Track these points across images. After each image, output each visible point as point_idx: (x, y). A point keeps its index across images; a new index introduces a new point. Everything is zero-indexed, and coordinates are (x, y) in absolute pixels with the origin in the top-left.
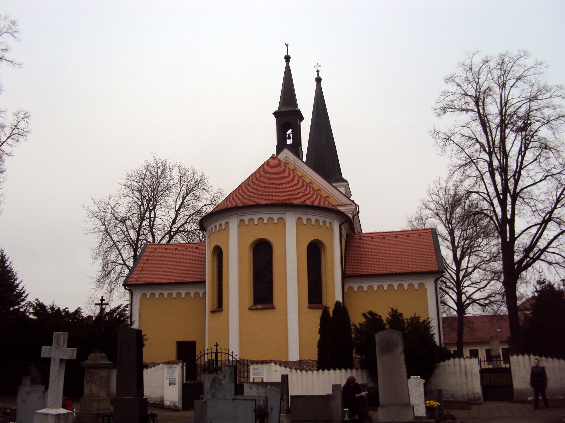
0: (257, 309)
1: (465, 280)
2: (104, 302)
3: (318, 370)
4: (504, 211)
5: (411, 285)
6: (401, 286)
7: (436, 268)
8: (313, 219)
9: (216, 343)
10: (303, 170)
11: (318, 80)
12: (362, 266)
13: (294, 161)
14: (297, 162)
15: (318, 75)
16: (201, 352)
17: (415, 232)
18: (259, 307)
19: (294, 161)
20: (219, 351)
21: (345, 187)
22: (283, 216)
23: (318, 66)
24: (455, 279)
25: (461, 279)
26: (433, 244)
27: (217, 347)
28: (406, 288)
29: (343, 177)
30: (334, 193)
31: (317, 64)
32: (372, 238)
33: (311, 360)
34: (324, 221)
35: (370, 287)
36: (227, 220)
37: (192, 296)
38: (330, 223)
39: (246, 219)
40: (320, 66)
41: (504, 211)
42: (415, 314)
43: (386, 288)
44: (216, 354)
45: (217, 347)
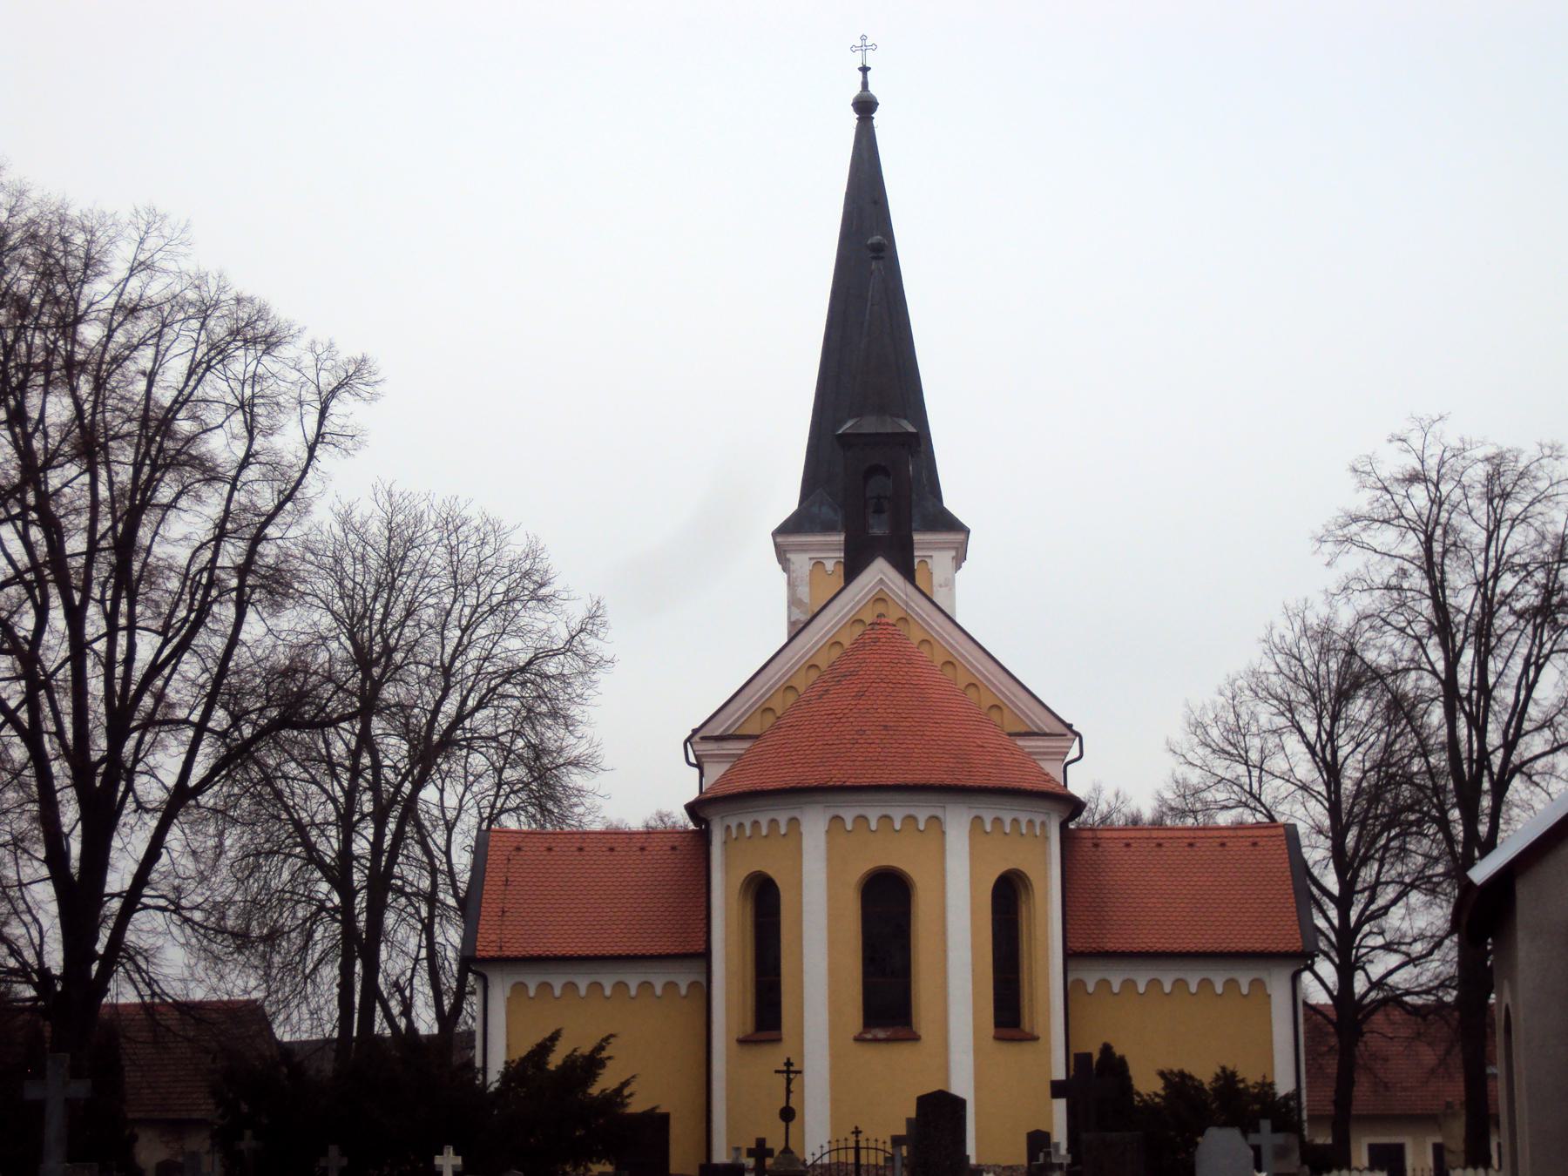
0: (876, 1040)
1: (1366, 928)
2: (792, 1069)
3: (1465, 1168)
4: (1470, 819)
5: (1231, 984)
6: (1206, 983)
7: (1296, 944)
8: (1007, 818)
9: (856, 1128)
10: (928, 624)
11: (865, 107)
12: (1108, 936)
13: (904, 597)
14: (913, 601)
15: (865, 85)
16: (822, 1147)
17: (1240, 833)
18: (881, 1034)
19: (904, 597)
20: (863, 1144)
21: (957, 549)
22: (939, 813)
23: (864, 46)
24: (1336, 922)
25: (1352, 925)
26: (1289, 874)
27: (857, 1136)
28: (1219, 990)
29: (946, 504)
30: (1015, 696)
31: (863, 38)
32: (1128, 845)
33: (999, 1166)
34: (1031, 822)
35: (1129, 984)
36: (795, 813)
37: (659, 991)
38: (1043, 824)
39: (849, 815)
40: (874, 47)
41: (1470, 819)
42: (1264, 1077)
43: (1167, 989)
44: (857, 1149)
45: (857, 1136)
